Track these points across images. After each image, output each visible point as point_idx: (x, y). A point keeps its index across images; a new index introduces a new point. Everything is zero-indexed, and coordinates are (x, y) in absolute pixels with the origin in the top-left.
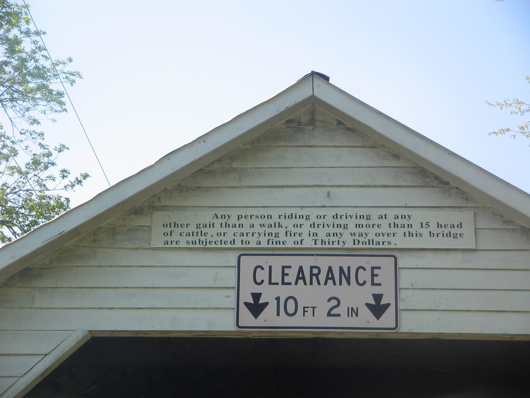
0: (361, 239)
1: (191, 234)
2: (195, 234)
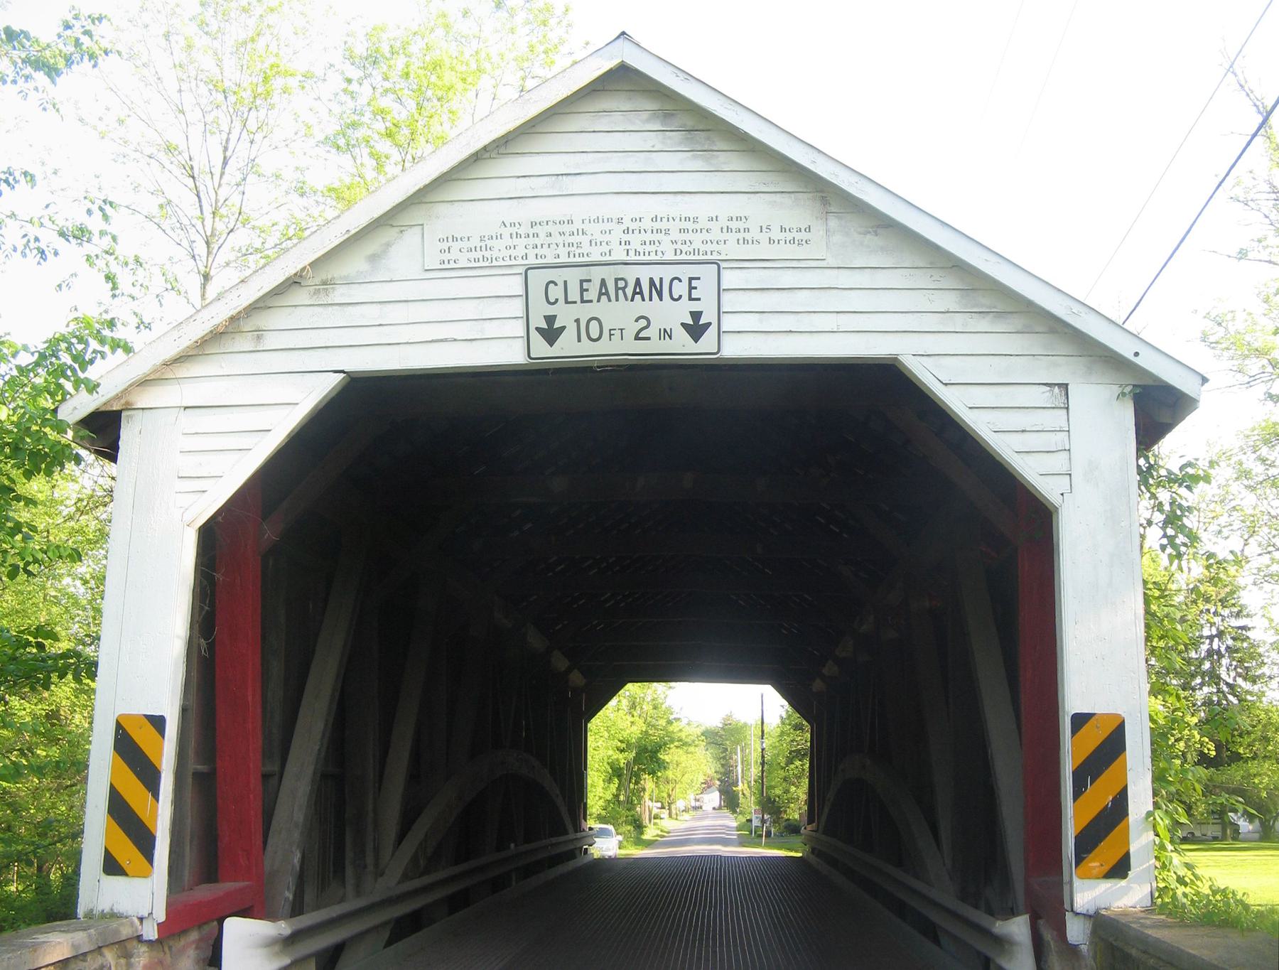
0: (685, 248)
1: (473, 250)
2: (478, 249)
